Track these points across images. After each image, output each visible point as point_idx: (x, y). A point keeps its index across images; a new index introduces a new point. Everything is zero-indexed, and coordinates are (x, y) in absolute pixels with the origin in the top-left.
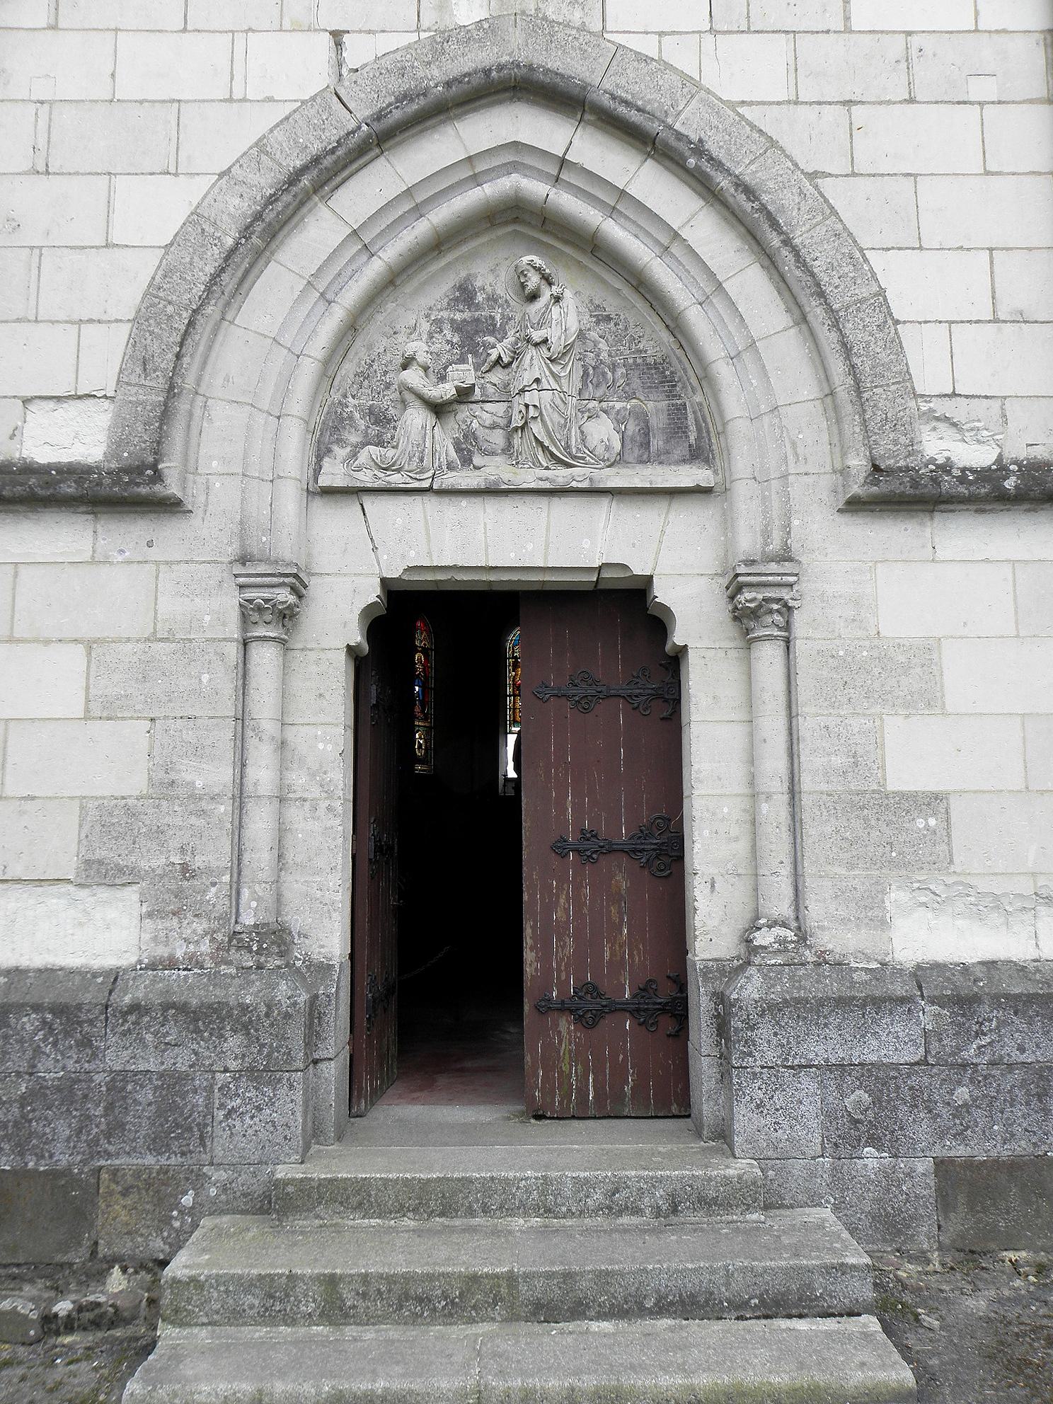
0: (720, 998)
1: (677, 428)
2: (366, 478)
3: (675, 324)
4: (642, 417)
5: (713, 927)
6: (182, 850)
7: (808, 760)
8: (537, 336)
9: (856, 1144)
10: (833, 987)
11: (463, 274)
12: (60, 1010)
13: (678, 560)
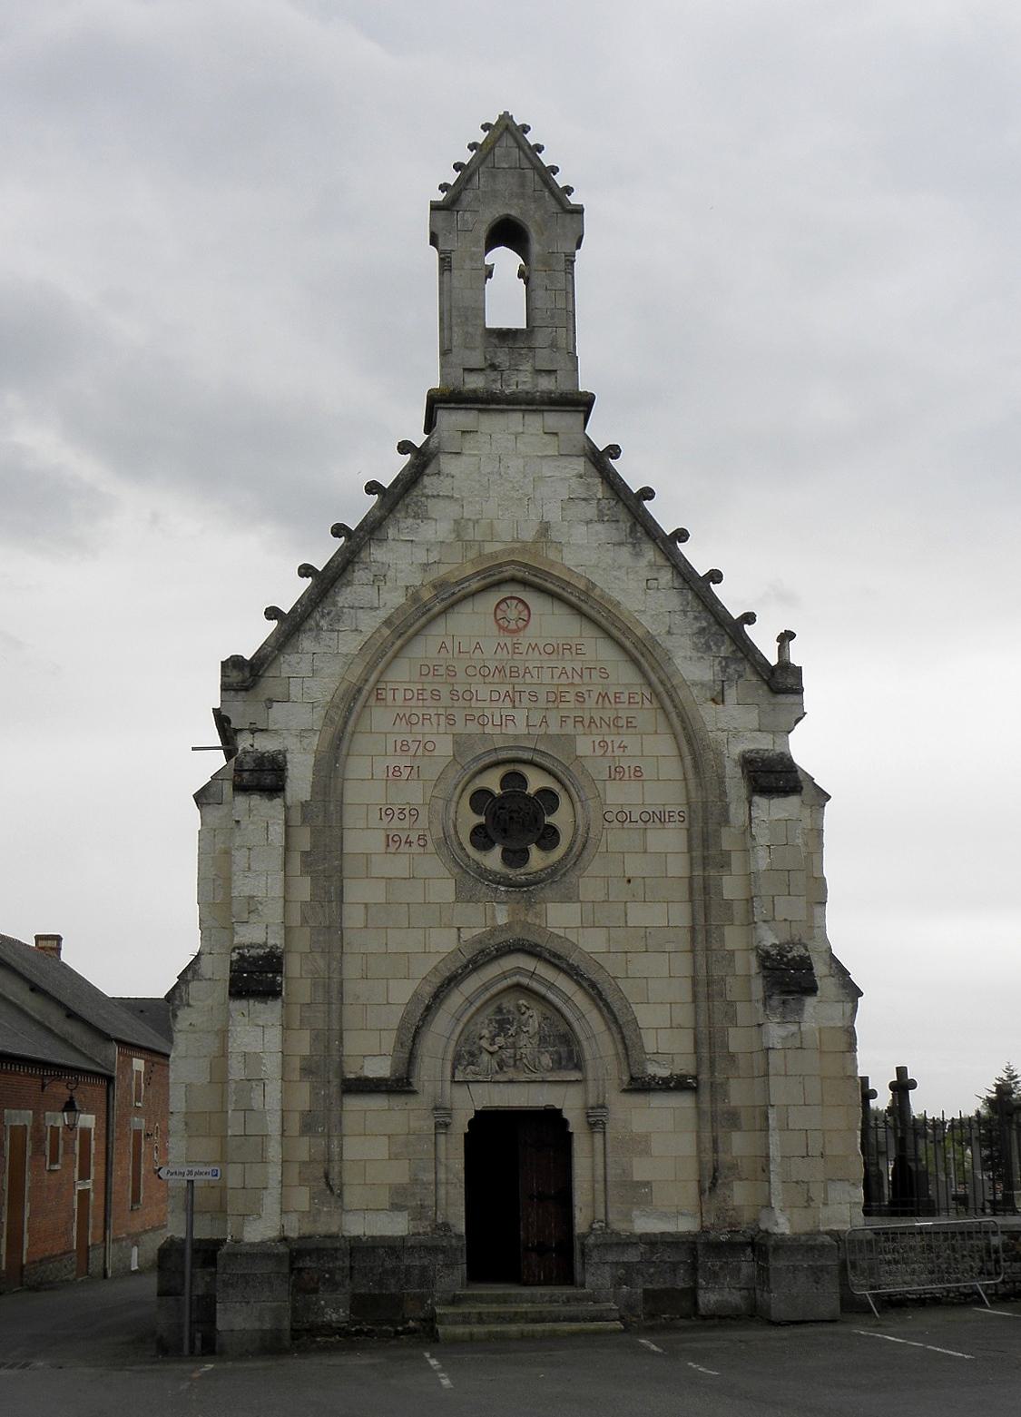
0: (582, 1244)
1: (570, 1057)
2: (470, 1078)
3: (569, 1024)
4: (557, 1052)
5: (581, 1221)
6: (421, 1200)
7: (611, 1172)
8: (525, 1029)
9: (620, 1285)
10: (615, 1240)
11: (499, 1003)
12: (390, 1247)
13: (570, 1103)
